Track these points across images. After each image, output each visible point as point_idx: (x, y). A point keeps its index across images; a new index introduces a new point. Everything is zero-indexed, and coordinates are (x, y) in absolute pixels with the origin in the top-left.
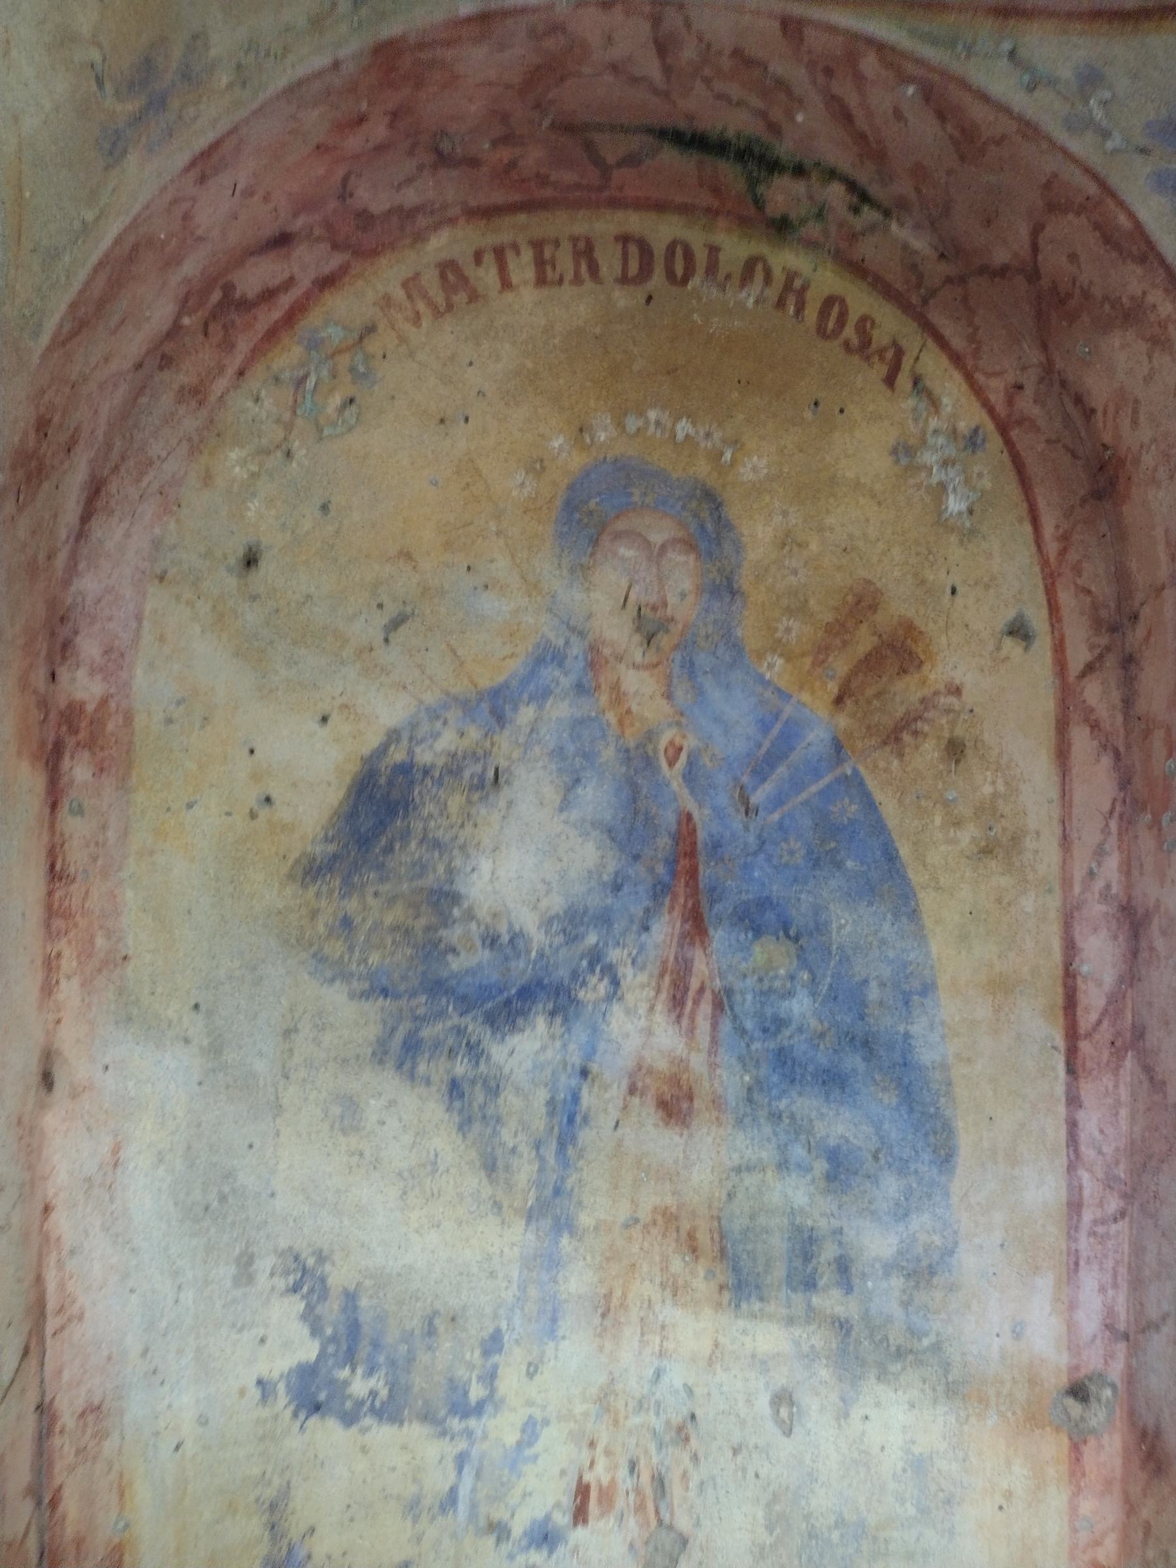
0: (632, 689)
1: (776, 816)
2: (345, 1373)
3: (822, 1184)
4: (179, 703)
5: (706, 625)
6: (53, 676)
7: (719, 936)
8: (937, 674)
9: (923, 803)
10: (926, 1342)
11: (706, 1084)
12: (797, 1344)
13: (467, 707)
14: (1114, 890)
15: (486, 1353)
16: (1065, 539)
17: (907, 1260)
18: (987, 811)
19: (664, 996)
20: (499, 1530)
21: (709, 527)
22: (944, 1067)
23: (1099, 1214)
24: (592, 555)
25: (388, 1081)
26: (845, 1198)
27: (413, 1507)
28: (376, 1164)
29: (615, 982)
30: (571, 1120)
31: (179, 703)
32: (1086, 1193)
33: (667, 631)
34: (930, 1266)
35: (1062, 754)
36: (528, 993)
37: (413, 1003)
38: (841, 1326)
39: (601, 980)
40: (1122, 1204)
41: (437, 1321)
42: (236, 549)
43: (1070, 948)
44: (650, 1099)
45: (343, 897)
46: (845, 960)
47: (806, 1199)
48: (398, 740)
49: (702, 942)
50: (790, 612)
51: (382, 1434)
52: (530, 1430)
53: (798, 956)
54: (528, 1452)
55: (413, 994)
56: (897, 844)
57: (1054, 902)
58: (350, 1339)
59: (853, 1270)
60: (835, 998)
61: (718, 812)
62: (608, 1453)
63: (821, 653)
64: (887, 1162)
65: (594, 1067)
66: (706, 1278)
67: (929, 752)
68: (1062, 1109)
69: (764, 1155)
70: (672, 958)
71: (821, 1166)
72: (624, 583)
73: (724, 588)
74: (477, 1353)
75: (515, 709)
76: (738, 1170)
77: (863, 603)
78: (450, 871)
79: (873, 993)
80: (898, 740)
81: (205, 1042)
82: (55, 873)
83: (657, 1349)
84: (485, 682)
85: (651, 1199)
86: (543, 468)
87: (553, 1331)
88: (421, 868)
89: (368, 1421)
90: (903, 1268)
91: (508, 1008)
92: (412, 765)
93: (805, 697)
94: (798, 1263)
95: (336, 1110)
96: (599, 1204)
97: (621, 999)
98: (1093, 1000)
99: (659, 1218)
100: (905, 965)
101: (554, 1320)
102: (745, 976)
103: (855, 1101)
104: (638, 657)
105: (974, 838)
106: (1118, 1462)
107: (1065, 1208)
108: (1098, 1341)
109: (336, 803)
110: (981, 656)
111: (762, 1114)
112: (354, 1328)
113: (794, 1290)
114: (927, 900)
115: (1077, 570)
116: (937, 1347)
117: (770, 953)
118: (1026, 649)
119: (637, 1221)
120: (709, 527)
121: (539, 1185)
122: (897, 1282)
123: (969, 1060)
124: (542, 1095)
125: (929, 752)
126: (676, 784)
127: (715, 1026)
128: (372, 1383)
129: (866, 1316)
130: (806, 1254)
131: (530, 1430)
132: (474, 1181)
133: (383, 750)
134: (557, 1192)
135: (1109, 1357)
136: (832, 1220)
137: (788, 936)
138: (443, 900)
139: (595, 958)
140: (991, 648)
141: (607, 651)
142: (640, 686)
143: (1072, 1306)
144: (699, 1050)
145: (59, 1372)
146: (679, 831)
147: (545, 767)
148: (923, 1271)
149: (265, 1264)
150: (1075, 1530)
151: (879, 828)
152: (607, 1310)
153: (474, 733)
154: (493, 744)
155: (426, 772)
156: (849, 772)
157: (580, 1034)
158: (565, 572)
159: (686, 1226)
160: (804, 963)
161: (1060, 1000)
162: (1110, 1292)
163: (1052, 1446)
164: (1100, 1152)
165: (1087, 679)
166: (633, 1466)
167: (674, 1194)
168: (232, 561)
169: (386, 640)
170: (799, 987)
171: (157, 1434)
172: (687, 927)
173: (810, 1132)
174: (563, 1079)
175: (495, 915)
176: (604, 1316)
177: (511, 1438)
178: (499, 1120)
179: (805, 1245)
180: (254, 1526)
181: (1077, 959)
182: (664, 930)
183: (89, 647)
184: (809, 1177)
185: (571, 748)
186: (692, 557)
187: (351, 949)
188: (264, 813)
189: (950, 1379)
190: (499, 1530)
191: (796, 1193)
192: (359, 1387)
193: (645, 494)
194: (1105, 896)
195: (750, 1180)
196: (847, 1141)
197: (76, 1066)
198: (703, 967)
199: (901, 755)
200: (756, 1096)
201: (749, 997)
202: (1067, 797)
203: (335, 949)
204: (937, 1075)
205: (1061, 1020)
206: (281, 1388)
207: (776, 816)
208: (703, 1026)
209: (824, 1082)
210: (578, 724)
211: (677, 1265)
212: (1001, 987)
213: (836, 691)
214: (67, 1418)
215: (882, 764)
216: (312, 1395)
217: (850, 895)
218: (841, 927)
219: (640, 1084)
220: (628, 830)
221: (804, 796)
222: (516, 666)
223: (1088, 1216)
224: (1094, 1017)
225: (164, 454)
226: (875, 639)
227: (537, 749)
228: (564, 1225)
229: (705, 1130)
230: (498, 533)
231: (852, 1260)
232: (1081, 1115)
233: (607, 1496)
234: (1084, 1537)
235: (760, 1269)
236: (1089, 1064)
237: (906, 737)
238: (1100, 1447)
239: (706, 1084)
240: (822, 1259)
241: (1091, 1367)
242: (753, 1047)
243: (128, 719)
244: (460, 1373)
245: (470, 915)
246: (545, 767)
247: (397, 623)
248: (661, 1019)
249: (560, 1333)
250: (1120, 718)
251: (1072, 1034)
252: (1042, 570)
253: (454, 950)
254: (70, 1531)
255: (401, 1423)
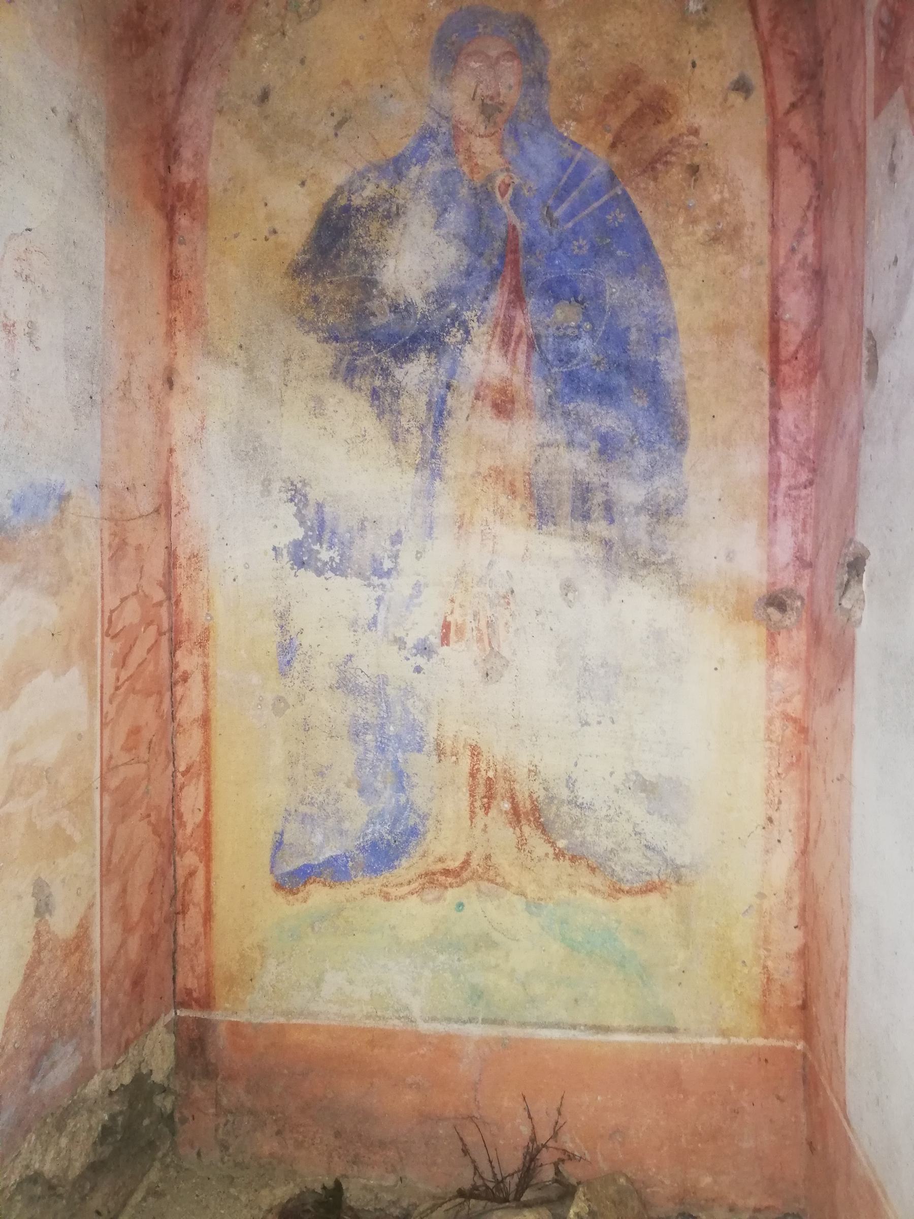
0: (479, 150)
1: (570, 225)
2: (317, 547)
3: (596, 456)
4: (230, 180)
5: (524, 104)
6: (169, 167)
7: (531, 302)
8: (681, 123)
9: (671, 209)
10: (664, 558)
11: (523, 394)
12: (577, 552)
13: (380, 169)
14: (810, 260)
15: (393, 543)
16: (775, 19)
17: (652, 506)
18: (716, 211)
19: (496, 340)
20: (400, 642)
21: (527, 42)
22: (682, 383)
23: (793, 482)
24: (455, 68)
25: (339, 389)
26: (611, 465)
27: (353, 625)
28: (333, 435)
29: (467, 332)
30: (441, 414)
31: (230, 180)
32: (784, 467)
33: (500, 111)
34: (667, 510)
35: (772, 169)
36: (415, 339)
37: (352, 344)
38: (606, 543)
39: (458, 331)
40: (811, 476)
41: (366, 523)
42: (257, 90)
43: (776, 301)
44: (488, 402)
45: (313, 285)
46: (614, 314)
47: (585, 464)
48: (342, 193)
49: (521, 307)
50: (580, 90)
51: (337, 581)
52: (418, 588)
53: (583, 313)
54: (416, 601)
55: (352, 339)
56: (653, 238)
57: (764, 271)
58: (320, 529)
59: (615, 509)
60: (607, 340)
61: (533, 225)
62: (461, 606)
63: (602, 114)
64: (640, 443)
65: (454, 383)
66: (521, 509)
67: (676, 174)
68: (766, 411)
69: (558, 437)
70: (502, 316)
71: (595, 445)
72: (473, 84)
73: (536, 81)
74: (388, 542)
75: (408, 168)
76: (542, 446)
77: (630, 79)
78: (371, 267)
79: (633, 336)
80: (654, 169)
81: (245, 366)
82: (173, 276)
83: (491, 549)
84: (391, 154)
85: (488, 461)
86: (424, 19)
87: (430, 534)
88: (355, 267)
89: (330, 574)
90: (649, 510)
91: (404, 346)
92: (350, 205)
93: (591, 146)
94: (579, 503)
95: (312, 404)
96: (457, 463)
97: (470, 342)
98: (792, 337)
99: (493, 475)
100: (655, 317)
101: (431, 528)
102: (548, 326)
103: (619, 405)
104: (482, 130)
105: (706, 231)
106: (804, 648)
107: (767, 476)
108: (791, 567)
109: (309, 231)
110: (714, 106)
111: (558, 413)
112: (322, 524)
113: (576, 520)
114: (672, 274)
115: (785, 39)
116: (671, 562)
117: (565, 314)
118: (746, 98)
119: (479, 473)
120: (527, 42)
121: (422, 451)
122: (644, 519)
123: (699, 378)
124: (424, 398)
125: (676, 174)
126: (506, 209)
127: (528, 357)
128: (331, 553)
129: (623, 538)
130: (584, 498)
131: (418, 588)
132: (386, 446)
133: (334, 199)
134: (433, 455)
135: (798, 578)
136: (602, 479)
137: (577, 301)
138: (368, 284)
139: (455, 317)
140: (720, 99)
141: (463, 128)
142: (485, 151)
143: (771, 543)
144: (518, 373)
145: (179, 535)
146: (507, 237)
147: (425, 203)
148: (661, 512)
149: (276, 485)
150: (770, 690)
151: (641, 228)
152: (461, 524)
153: (385, 185)
154: (395, 190)
155: (358, 210)
156: (620, 193)
157: (446, 362)
158: (438, 82)
159: (509, 478)
160: (587, 317)
161: (767, 338)
162: (801, 536)
163: (755, 633)
164: (795, 441)
165: (792, 114)
166: (475, 615)
167: (502, 459)
168: (255, 98)
169: (336, 135)
170: (583, 333)
171: (225, 571)
172: (512, 296)
173: (589, 424)
174: (436, 389)
175: (396, 293)
176: (460, 527)
177: (407, 591)
178: (399, 413)
179: (583, 492)
180: (270, 626)
181: (781, 310)
182: (497, 300)
183: (187, 154)
184: (587, 452)
185: (441, 190)
186: (516, 63)
187: (318, 314)
188: (272, 238)
189: (681, 583)
190: (400, 642)
191: (579, 461)
192: (325, 555)
193: (485, 27)
194: (803, 265)
195: (549, 452)
196: (614, 430)
197: (184, 378)
198: (522, 322)
199: (655, 179)
200: (554, 400)
201: (551, 339)
202: (775, 198)
203: (310, 314)
204: (676, 388)
205: (767, 351)
206: (285, 552)
207: (570, 225)
208: (521, 358)
209: (599, 393)
210: (446, 174)
211: (503, 500)
212: (723, 330)
213: (611, 139)
214: (182, 560)
215: (642, 185)
216: (301, 557)
217: (619, 273)
218: (612, 294)
219: (482, 393)
220: (475, 240)
221: (589, 210)
222: (409, 142)
223: (784, 484)
224: (792, 348)
225: (221, 43)
226: (638, 103)
227: (421, 192)
228: (437, 474)
229: (522, 421)
230: (398, 63)
231: (614, 503)
232: (780, 415)
233: (460, 631)
234: (777, 695)
235: (554, 506)
236: (787, 381)
237: (659, 166)
238: (790, 638)
239: (523, 394)
240: (595, 502)
241: (785, 584)
242: (553, 371)
243: (206, 189)
244: (379, 552)
245: (383, 294)
246: (425, 203)
247: (340, 124)
248: (495, 354)
249: (434, 535)
250: (816, 138)
251: (775, 362)
252: (758, 43)
253: (374, 314)
254: (185, 617)
255: (346, 577)
